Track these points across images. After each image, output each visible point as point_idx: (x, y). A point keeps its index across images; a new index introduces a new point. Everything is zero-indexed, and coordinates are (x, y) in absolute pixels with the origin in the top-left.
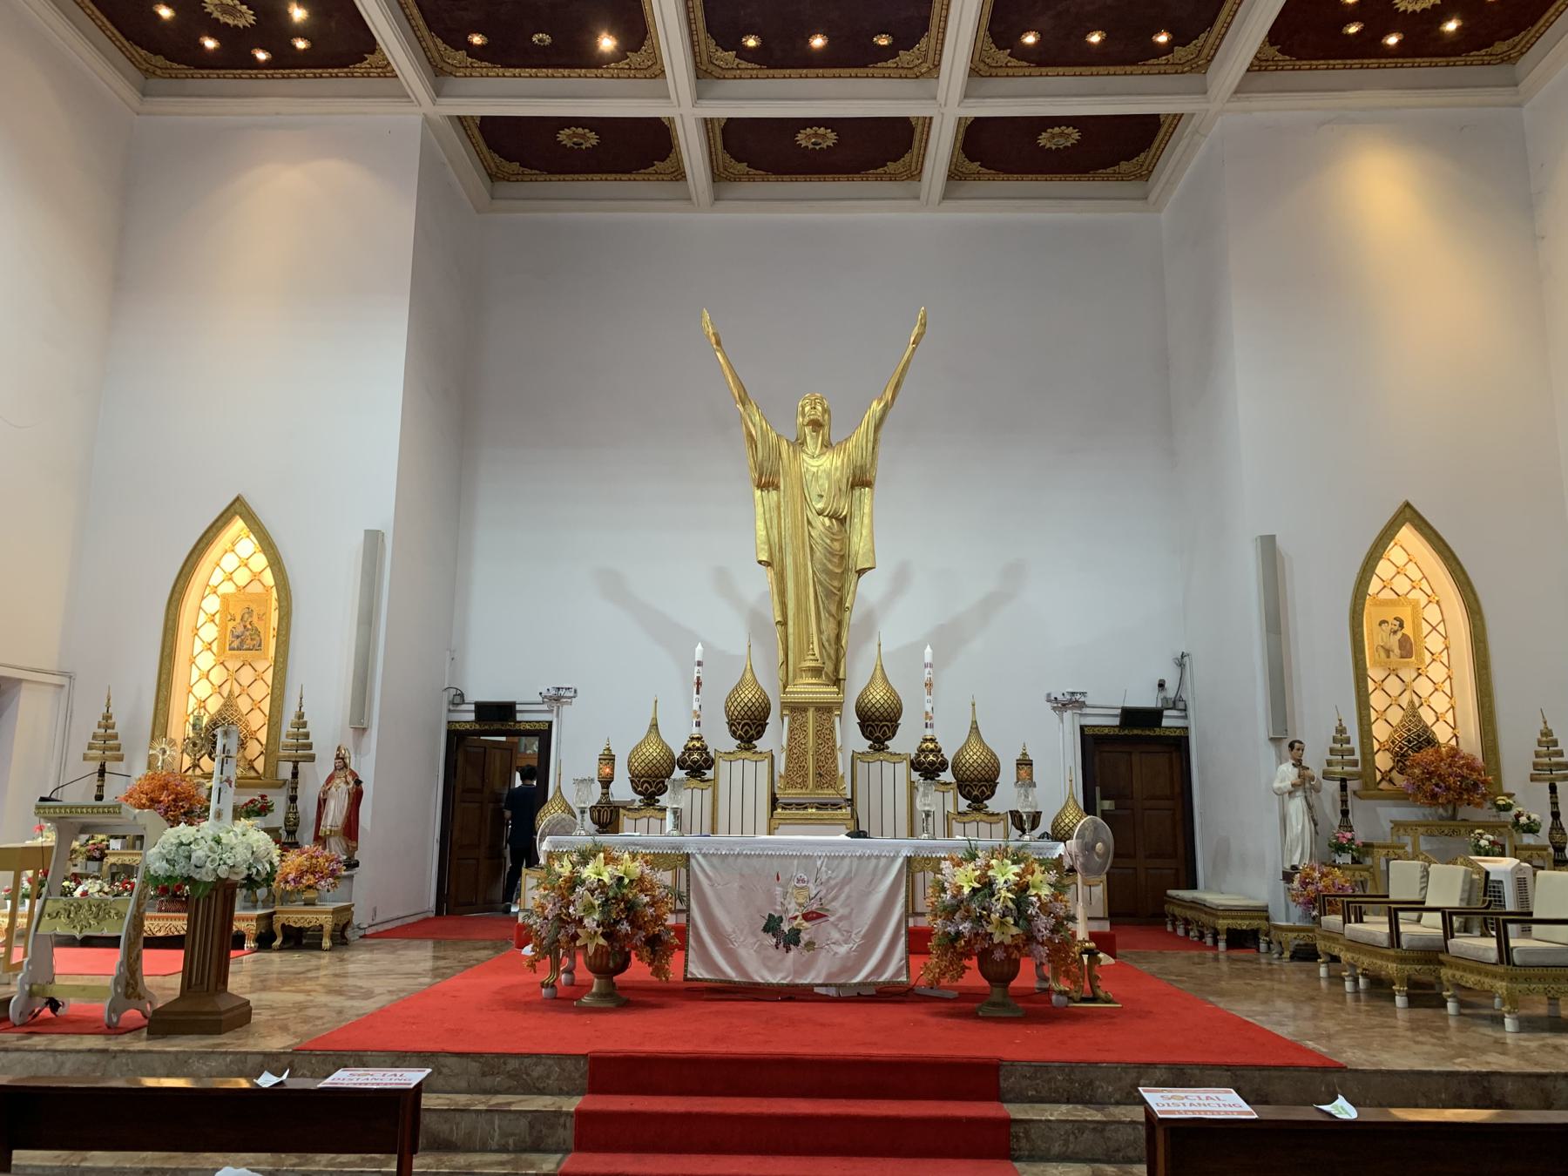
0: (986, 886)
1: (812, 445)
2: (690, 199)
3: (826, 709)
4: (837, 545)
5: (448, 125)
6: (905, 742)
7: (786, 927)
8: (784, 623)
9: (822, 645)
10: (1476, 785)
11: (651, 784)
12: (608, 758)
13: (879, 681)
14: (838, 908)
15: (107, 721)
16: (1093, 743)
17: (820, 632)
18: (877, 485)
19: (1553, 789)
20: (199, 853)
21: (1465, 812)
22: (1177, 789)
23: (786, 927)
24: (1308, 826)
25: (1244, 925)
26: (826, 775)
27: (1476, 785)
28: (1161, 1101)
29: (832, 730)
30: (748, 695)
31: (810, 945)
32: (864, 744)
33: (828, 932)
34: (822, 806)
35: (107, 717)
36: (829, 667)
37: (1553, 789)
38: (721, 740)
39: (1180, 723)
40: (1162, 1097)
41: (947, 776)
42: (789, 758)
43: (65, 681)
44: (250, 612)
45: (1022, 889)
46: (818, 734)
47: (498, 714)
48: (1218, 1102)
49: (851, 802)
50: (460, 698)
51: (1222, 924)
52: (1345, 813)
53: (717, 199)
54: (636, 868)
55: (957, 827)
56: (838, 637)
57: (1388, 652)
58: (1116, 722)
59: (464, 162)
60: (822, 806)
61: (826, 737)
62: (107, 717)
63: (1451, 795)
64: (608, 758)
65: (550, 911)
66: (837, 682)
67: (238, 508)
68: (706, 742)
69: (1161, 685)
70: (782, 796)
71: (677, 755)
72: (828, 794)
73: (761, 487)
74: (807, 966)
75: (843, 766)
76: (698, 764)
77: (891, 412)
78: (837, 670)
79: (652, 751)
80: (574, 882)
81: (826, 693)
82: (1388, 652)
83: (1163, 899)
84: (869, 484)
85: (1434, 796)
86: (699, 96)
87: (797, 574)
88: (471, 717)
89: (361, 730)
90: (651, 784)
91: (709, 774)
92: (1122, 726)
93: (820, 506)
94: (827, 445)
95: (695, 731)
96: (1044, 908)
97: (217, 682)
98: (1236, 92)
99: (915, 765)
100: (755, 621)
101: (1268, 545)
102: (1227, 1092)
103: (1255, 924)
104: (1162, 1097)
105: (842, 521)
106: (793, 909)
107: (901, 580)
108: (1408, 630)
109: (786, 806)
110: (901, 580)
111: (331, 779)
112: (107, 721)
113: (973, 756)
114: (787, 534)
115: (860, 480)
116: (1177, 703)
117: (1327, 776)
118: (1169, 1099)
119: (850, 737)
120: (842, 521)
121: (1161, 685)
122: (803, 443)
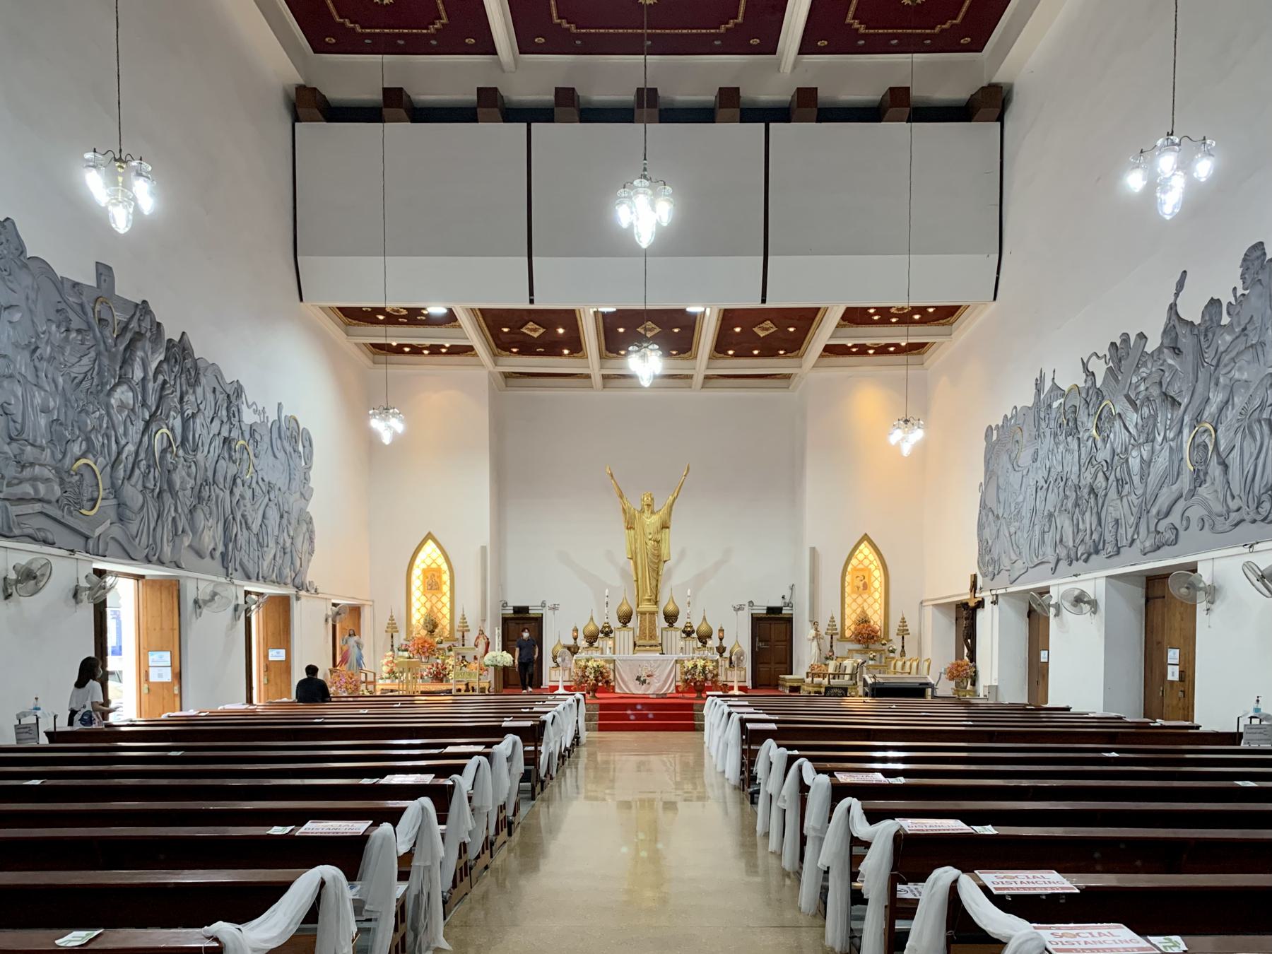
0: (696, 666)
1: (647, 513)
2: (592, 387)
3: (653, 613)
4: (656, 552)
5: (499, 375)
6: (680, 624)
7: (642, 679)
8: (637, 581)
9: (651, 589)
10: (873, 637)
11: (592, 639)
12: (576, 630)
13: (671, 602)
14: (656, 674)
15: (392, 619)
16: (756, 620)
17: (650, 584)
18: (671, 528)
19: (903, 638)
20: (499, 659)
21: (871, 646)
22: (788, 637)
23: (642, 679)
24: (818, 651)
25: (795, 684)
26: (652, 637)
27: (873, 637)
28: (1052, 938)
29: (655, 621)
30: (625, 608)
31: (649, 683)
32: (666, 625)
33: (653, 680)
34: (651, 646)
35: (392, 617)
36: (653, 597)
37: (903, 638)
38: (615, 624)
39: (790, 612)
40: (1052, 934)
41: (695, 635)
42: (640, 630)
43: (371, 603)
44: (434, 575)
45: (704, 667)
46: (650, 622)
47: (521, 611)
48: (1114, 938)
49: (661, 644)
50: (505, 605)
51: (788, 684)
52: (831, 647)
53: (604, 387)
54: (602, 663)
55: (697, 652)
56: (657, 586)
57: (858, 588)
58: (765, 612)
59: (500, 379)
60: (651, 646)
61: (652, 623)
62: (392, 617)
63: (865, 640)
64: (576, 630)
65: (580, 674)
66: (656, 603)
67: (429, 536)
68: (610, 624)
69: (783, 597)
70: (638, 643)
71: (600, 628)
72: (653, 642)
73: (628, 528)
74: (648, 689)
75: (658, 632)
76: (607, 633)
77: (676, 501)
78: (656, 597)
79: (592, 628)
80: (586, 667)
81: (652, 608)
82: (858, 588)
83: (778, 679)
84: (668, 528)
85: (860, 641)
86: (602, 367)
87: (642, 563)
88: (512, 612)
89: (484, 620)
90: (592, 639)
91: (612, 635)
92: (767, 613)
93: (650, 537)
94: (653, 513)
95: (606, 620)
96: (710, 671)
97: (423, 602)
98: (814, 367)
99: (684, 632)
100: (624, 574)
101: (813, 550)
102: (1117, 927)
103: (799, 684)
104: (1052, 934)
105: (658, 542)
106: (644, 674)
107: (682, 554)
108: (866, 580)
109: (639, 646)
110: (682, 554)
111: (478, 638)
112: (392, 619)
113: (704, 628)
114: (638, 546)
115: (665, 526)
116: (789, 605)
117: (826, 633)
118: (1061, 937)
119: (661, 622)
120: (658, 542)
121: (783, 597)
122: (644, 512)
